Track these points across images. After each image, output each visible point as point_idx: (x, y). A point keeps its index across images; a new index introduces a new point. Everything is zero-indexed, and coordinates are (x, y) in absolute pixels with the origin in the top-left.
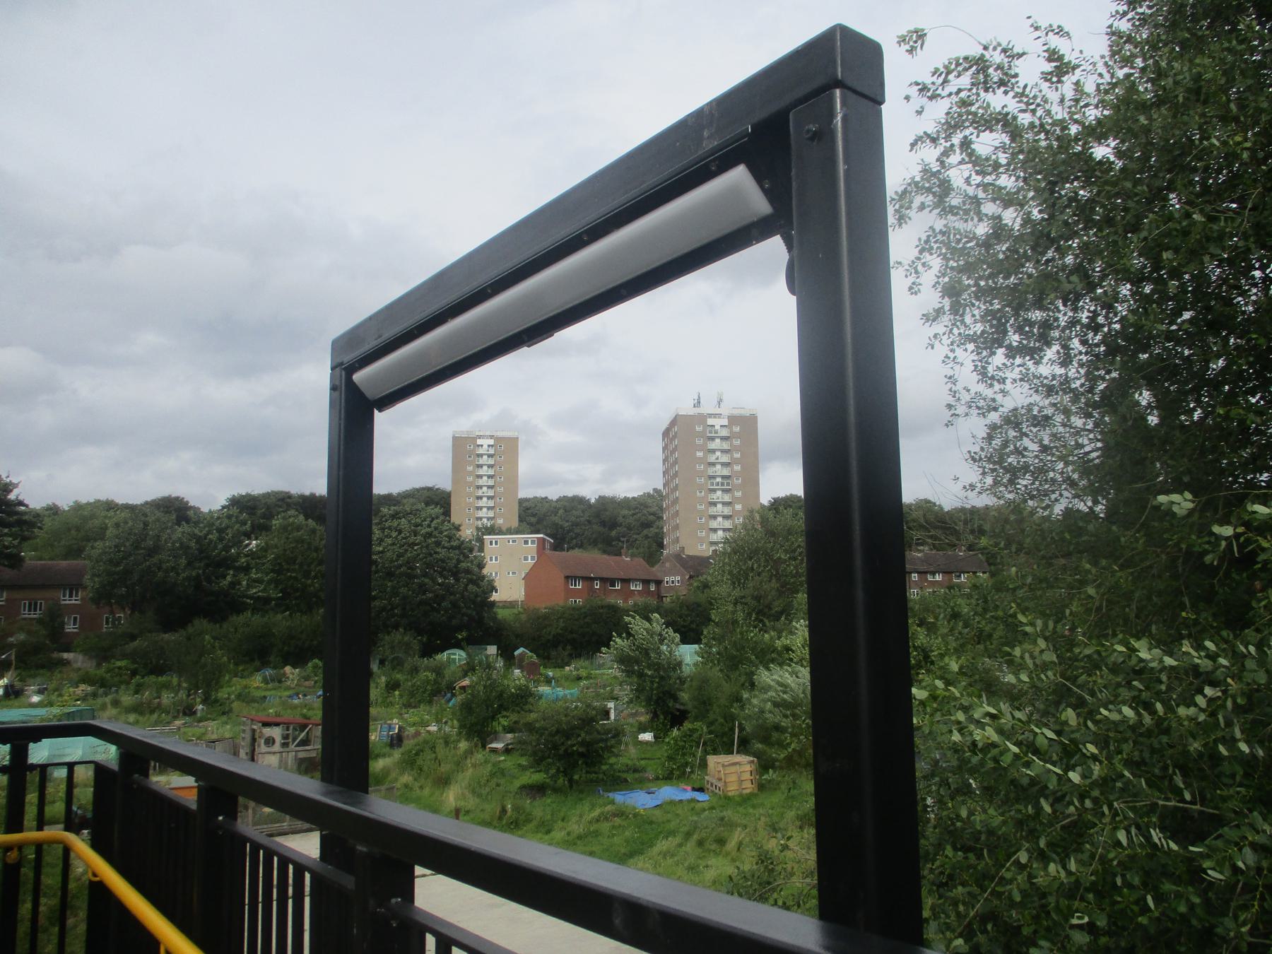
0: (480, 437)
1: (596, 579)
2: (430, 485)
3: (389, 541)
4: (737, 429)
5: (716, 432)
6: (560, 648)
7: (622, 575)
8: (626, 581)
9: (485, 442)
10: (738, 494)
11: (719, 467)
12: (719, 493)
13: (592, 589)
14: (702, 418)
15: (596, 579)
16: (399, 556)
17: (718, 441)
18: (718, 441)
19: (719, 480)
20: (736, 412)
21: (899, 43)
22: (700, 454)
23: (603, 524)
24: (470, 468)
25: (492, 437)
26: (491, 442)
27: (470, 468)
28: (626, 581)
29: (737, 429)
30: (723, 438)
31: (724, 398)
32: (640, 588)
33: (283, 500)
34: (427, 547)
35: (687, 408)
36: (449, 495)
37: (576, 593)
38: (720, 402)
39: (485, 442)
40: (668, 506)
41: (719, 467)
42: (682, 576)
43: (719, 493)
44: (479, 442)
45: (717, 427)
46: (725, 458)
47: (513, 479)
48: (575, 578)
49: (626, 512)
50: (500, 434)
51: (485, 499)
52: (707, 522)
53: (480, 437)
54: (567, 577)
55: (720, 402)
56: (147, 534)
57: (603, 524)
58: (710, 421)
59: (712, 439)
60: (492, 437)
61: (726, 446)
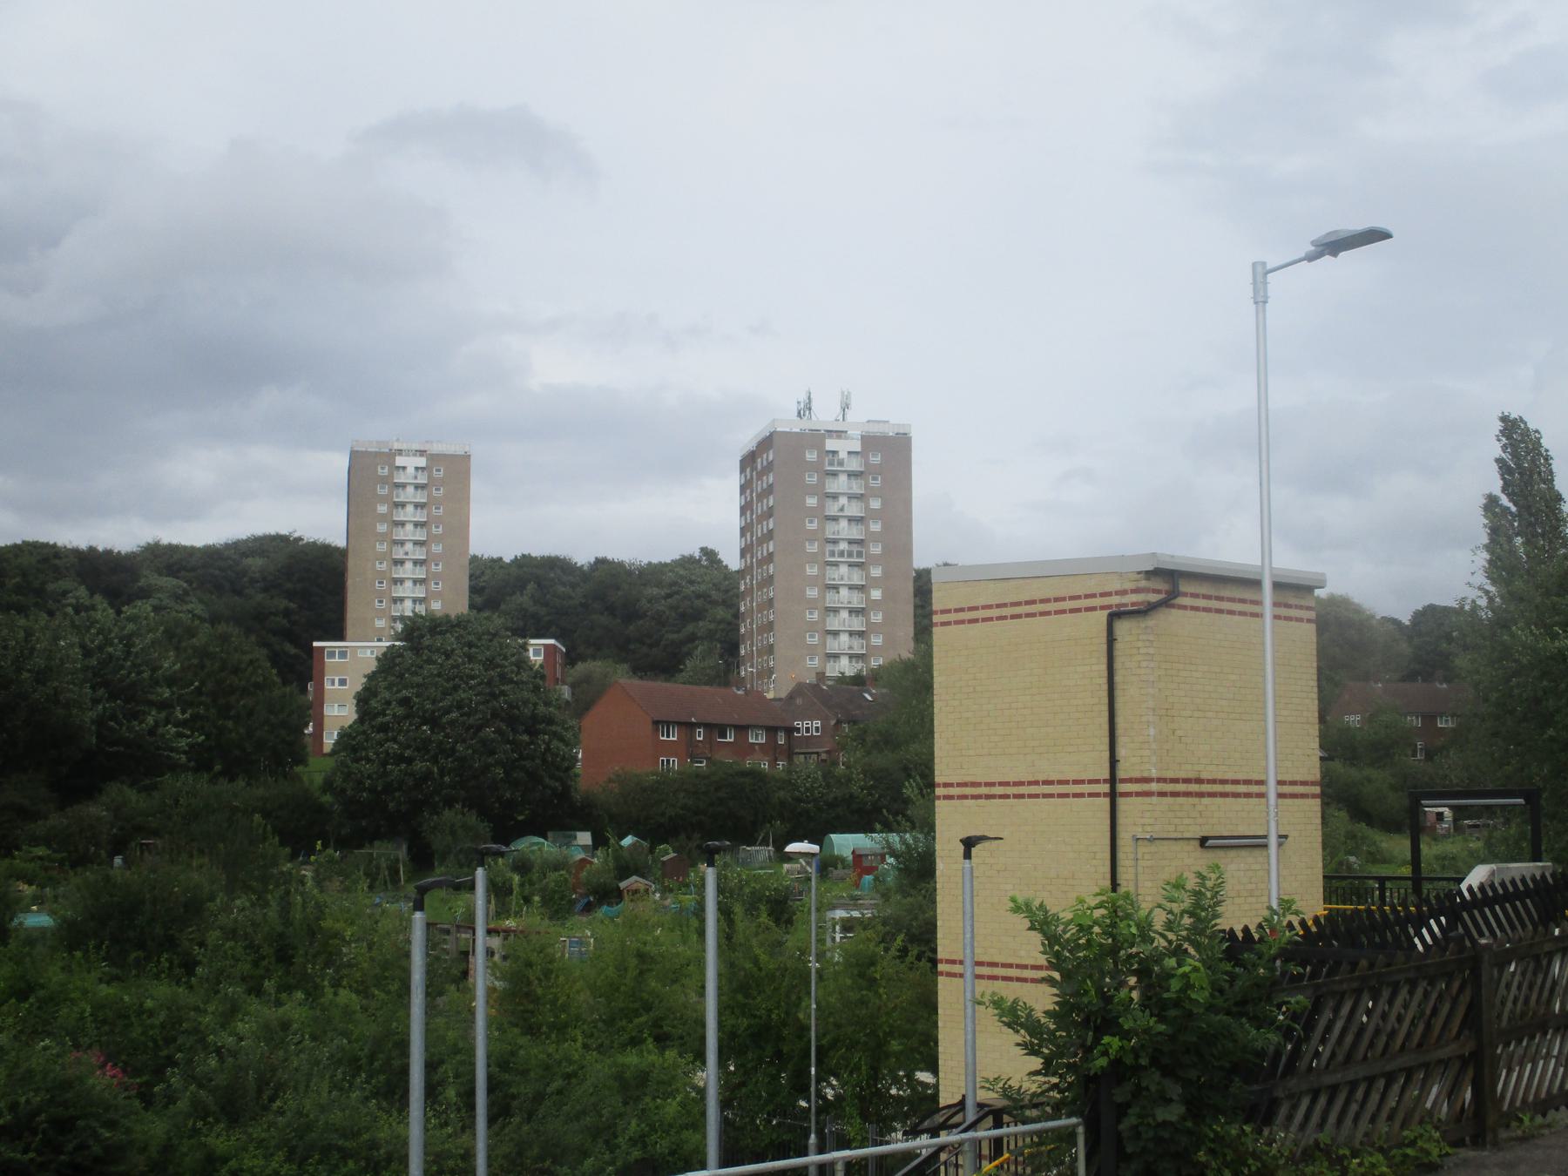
0: (400, 452)
1: (698, 725)
2: (284, 532)
3: (434, 669)
4: (876, 459)
5: (841, 463)
6: (683, 837)
7: (736, 719)
8: (742, 729)
9: (411, 463)
10: (876, 572)
11: (844, 523)
12: (844, 569)
13: (691, 742)
14: (815, 438)
15: (698, 725)
16: (445, 693)
17: (843, 478)
18: (843, 478)
19: (843, 546)
20: (876, 429)
21: (1504, 419)
22: (811, 501)
23: (611, 610)
24: (382, 509)
25: (422, 453)
26: (422, 462)
27: (382, 509)
28: (742, 729)
29: (876, 459)
30: (851, 475)
31: (853, 403)
32: (762, 740)
33: (45, 560)
34: (489, 683)
35: (788, 422)
36: (343, 553)
37: (669, 748)
38: (845, 407)
39: (411, 463)
40: (750, 591)
41: (844, 523)
42: (824, 720)
43: (844, 569)
44: (400, 461)
45: (843, 455)
46: (854, 509)
47: (460, 529)
48: (668, 723)
49: (655, 591)
50: (436, 448)
51: (409, 565)
52: (391, 493)
53: (400, 452)
54: (656, 723)
55: (845, 407)
56: (33, 649)
57: (611, 610)
58: (830, 444)
59: (834, 474)
60: (422, 453)
61: (857, 487)
